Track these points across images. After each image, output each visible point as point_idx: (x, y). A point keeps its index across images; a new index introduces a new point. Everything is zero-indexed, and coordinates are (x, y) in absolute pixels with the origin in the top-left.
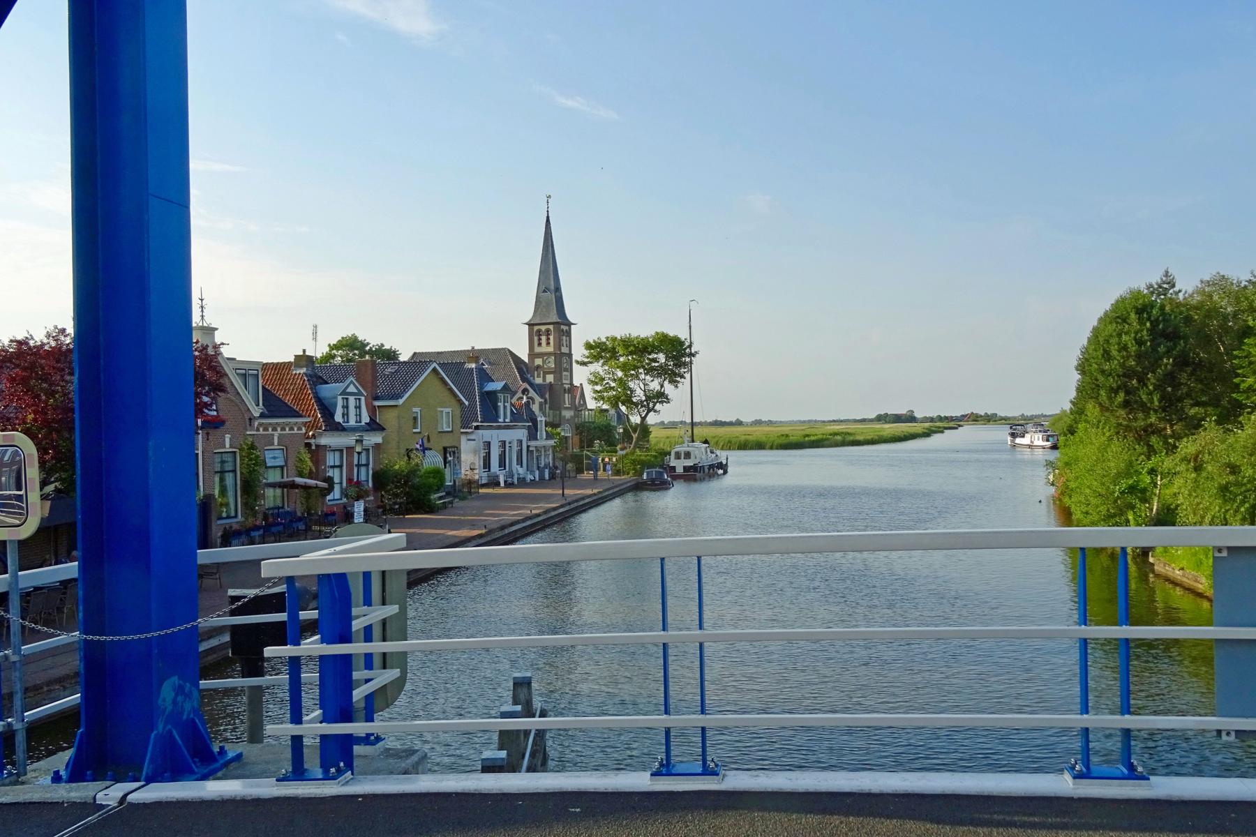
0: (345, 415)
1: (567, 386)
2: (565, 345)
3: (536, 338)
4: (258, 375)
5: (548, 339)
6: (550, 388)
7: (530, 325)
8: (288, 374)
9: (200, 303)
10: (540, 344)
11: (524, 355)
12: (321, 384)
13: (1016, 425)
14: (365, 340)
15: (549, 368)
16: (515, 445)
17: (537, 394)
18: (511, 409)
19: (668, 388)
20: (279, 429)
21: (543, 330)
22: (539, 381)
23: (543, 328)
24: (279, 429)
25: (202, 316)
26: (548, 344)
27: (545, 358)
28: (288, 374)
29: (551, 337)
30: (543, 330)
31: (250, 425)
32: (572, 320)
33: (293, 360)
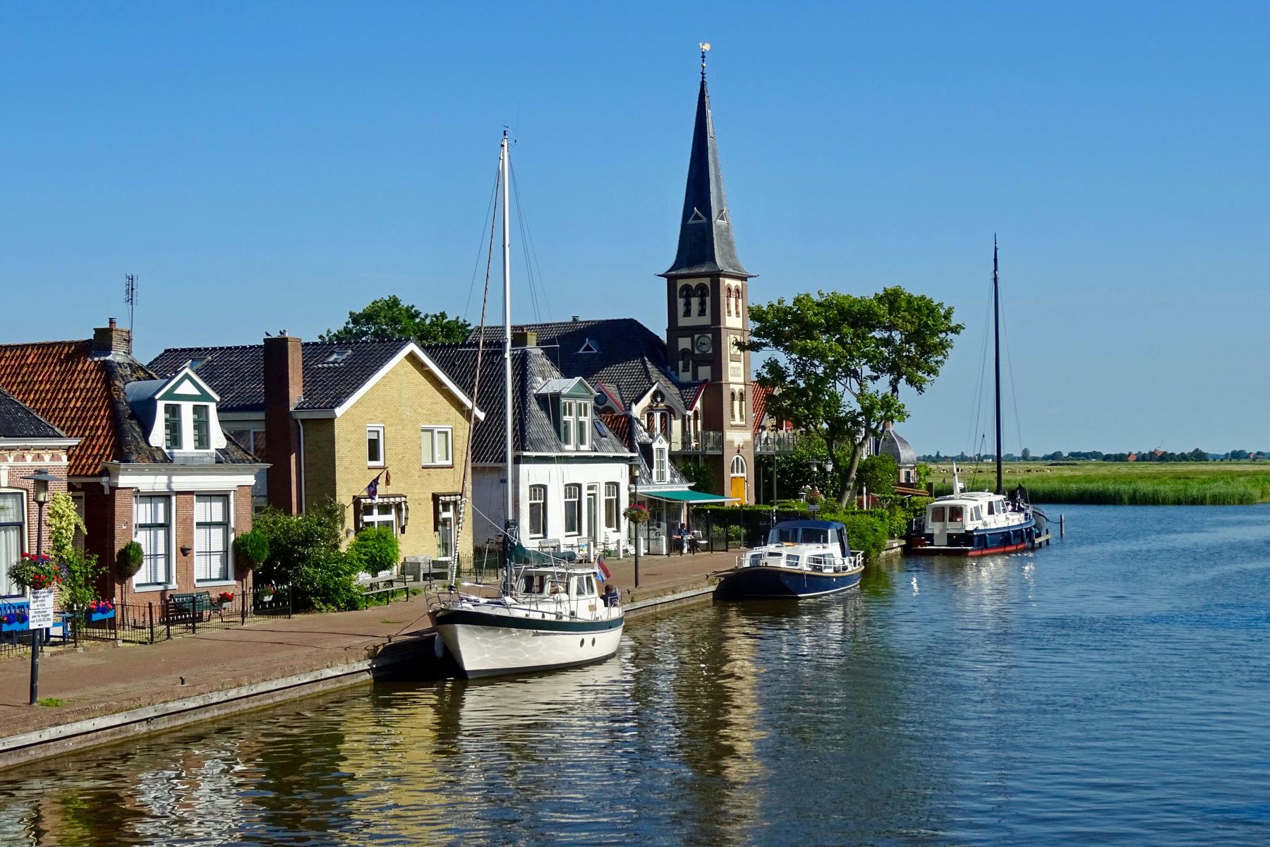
3: (681, 302)
5: (702, 303)
10: (687, 313)
13: (917, 495)
14: (413, 306)
15: (704, 354)
19: (906, 391)
21: (694, 287)
23: (694, 283)
27: (696, 336)
30: (694, 287)
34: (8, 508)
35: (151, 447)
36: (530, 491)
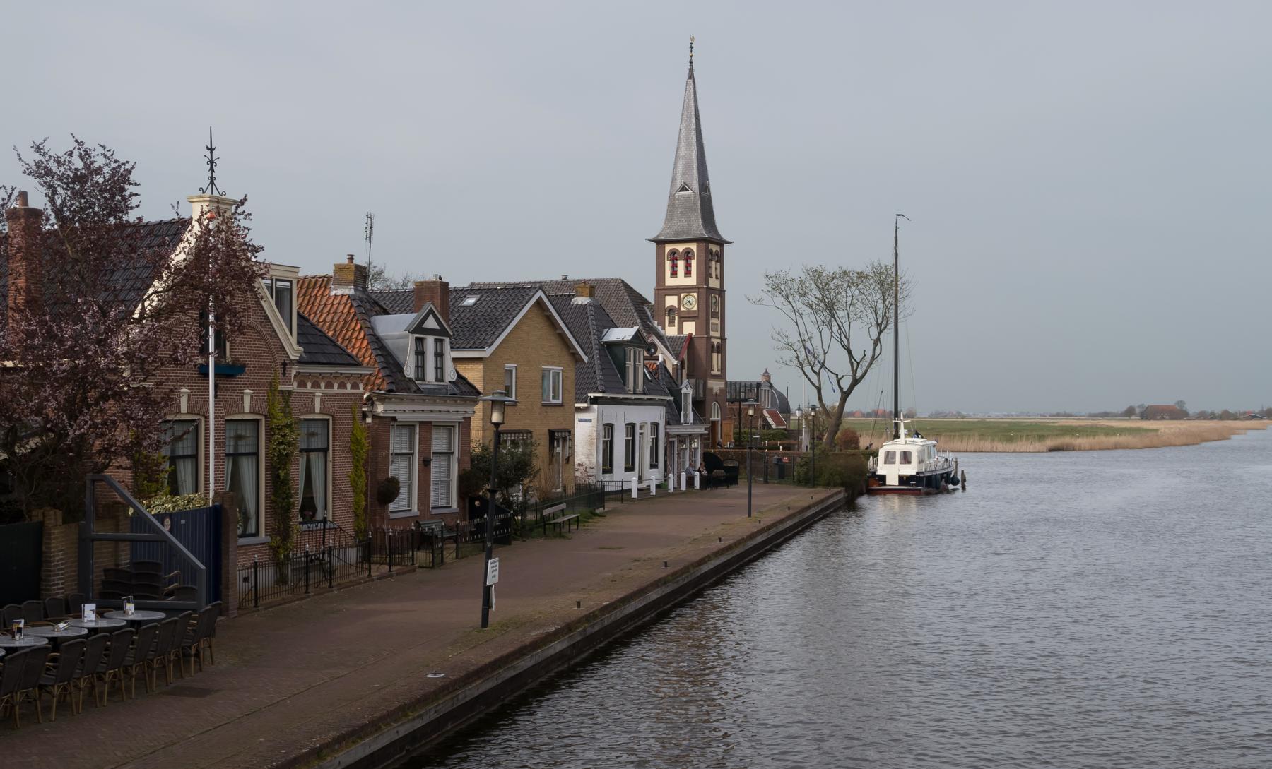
0: (420, 367)
1: (716, 342)
2: (714, 275)
3: (668, 264)
4: (291, 290)
5: (688, 266)
6: (688, 347)
7: (660, 243)
8: (322, 295)
9: (209, 156)
10: (674, 274)
11: (648, 291)
12: (377, 314)
15: (689, 311)
16: (648, 430)
17: (669, 351)
18: (644, 374)
20: (323, 385)
21: (681, 251)
22: (671, 331)
23: (681, 248)
24: (323, 385)
25: (212, 179)
26: (688, 273)
27: (682, 295)
28: (322, 295)
29: (694, 263)
30: (681, 251)
31: (284, 374)
32: (725, 236)
33: (331, 273)
34: (317, 434)
35: (405, 377)
36: (605, 429)
